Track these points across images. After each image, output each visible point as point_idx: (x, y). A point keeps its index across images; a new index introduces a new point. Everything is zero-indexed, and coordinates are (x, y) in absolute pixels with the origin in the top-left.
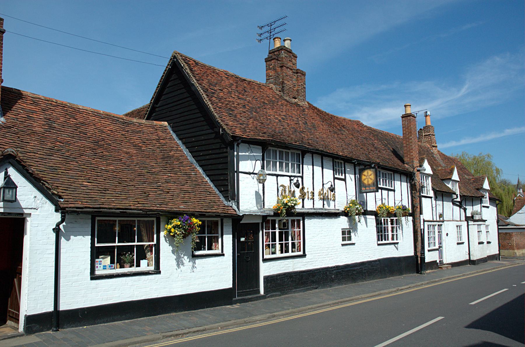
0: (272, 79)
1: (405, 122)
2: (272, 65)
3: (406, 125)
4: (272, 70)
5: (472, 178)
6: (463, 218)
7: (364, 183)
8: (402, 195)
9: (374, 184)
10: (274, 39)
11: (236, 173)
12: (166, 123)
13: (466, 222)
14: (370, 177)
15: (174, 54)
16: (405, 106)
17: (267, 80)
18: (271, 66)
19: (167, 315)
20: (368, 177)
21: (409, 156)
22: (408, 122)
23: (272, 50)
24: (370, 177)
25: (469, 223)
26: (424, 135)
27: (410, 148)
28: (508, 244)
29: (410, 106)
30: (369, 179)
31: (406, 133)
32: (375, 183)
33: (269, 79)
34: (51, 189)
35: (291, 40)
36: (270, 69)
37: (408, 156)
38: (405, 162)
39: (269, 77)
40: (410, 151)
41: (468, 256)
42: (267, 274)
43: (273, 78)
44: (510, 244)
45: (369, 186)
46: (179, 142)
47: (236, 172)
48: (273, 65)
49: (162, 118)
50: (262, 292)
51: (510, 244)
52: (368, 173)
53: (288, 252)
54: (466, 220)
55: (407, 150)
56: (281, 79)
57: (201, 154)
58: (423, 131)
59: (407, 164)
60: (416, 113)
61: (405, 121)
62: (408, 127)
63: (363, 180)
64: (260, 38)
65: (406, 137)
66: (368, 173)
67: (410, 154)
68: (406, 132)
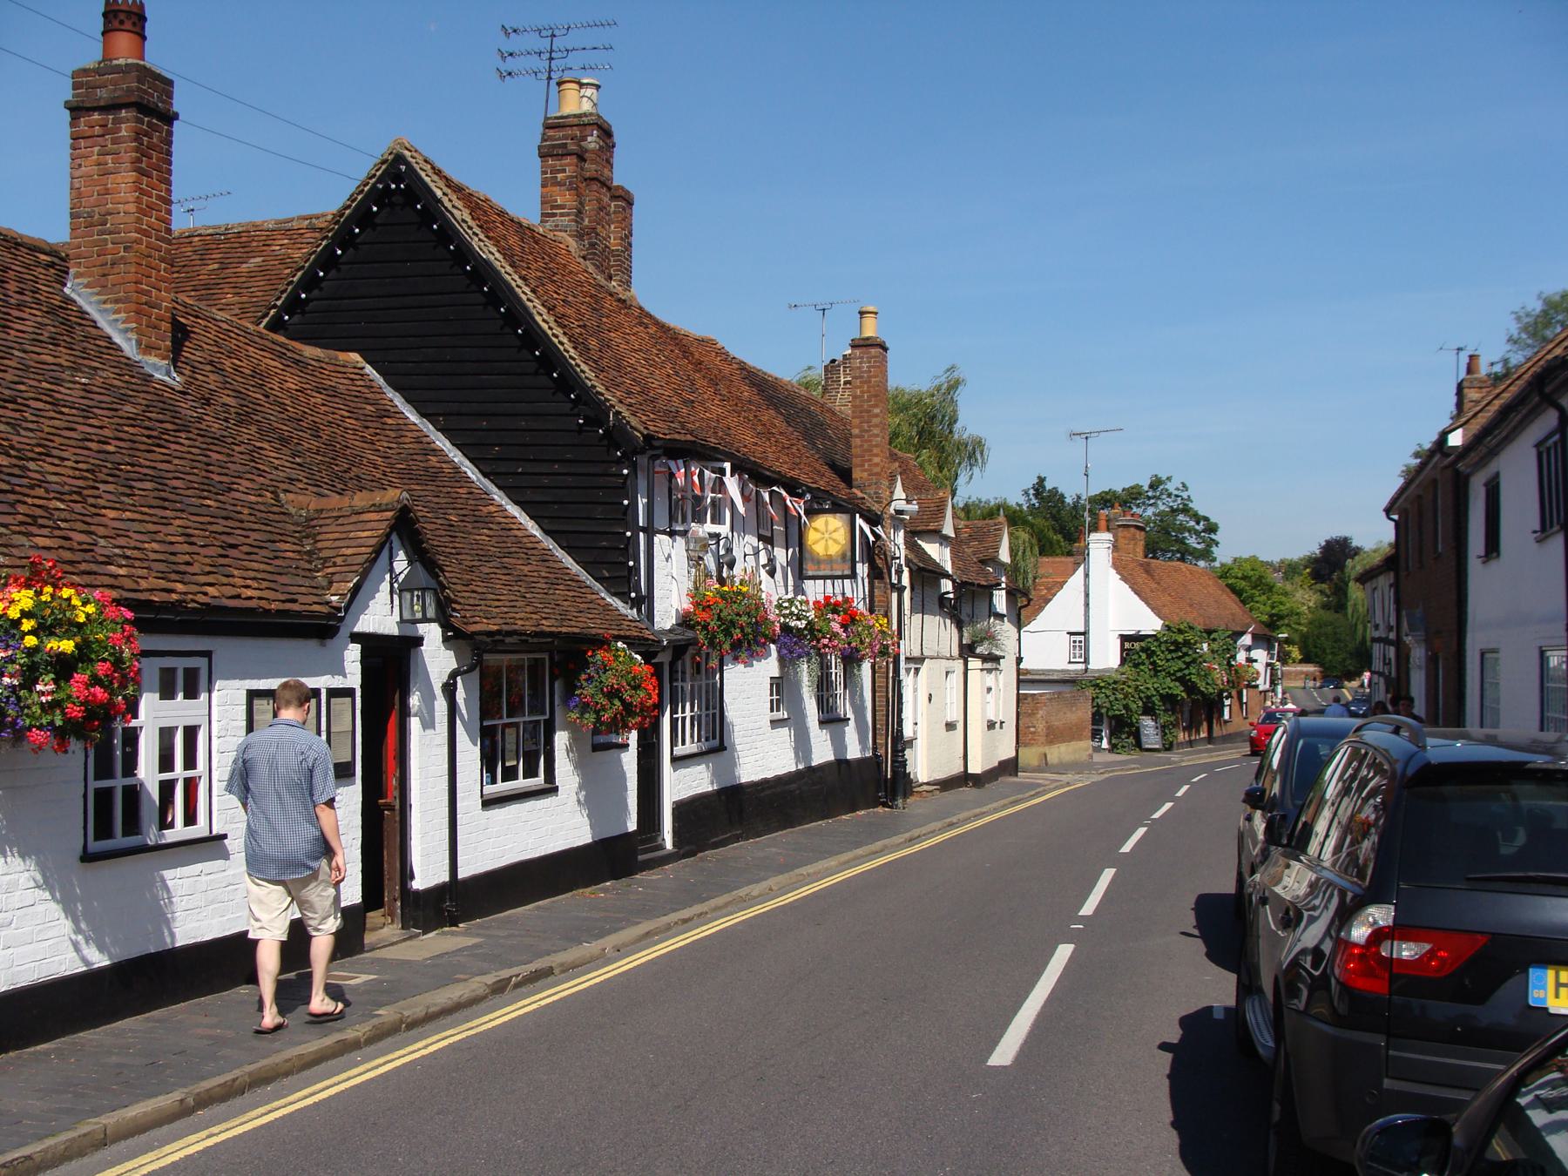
0: (562, 215)
1: (861, 363)
2: (564, 171)
3: (863, 372)
4: (562, 188)
5: (967, 527)
6: (956, 652)
7: (811, 552)
8: (1087, 605)
9: (844, 556)
10: (559, 84)
11: (641, 534)
12: (355, 357)
13: (962, 661)
14: (835, 535)
15: (398, 147)
16: (862, 313)
17: (543, 215)
18: (560, 176)
19: (564, 896)
20: (827, 536)
21: (866, 466)
22: (870, 362)
23: (556, 118)
24: (835, 535)
25: (970, 665)
26: (842, 380)
27: (870, 441)
28: (1029, 727)
29: (876, 313)
30: (830, 542)
31: (863, 396)
32: (849, 554)
33: (554, 215)
34: (446, 588)
35: (598, 87)
36: (560, 184)
37: (863, 465)
38: (854, 483)
39: (553, 207)
40: (871, 451)
41: (961, 762)
42: (677, 798)
43: (568, 214)
44: (1032, 729)
45: (830, 560)
46: (427, 427)
47: (644, 529)
48: (568, 174)
49: (311, 338)
50: (669, 845)
51: (1032, 729)
52: (827, 523)
53: (95, 789)
54: (961, 655)
55: (862, 446)
56: (587, 220)
57: (520, 470)
58: (842, 369)
59: (858, 487)
60: (822, 307)
61: (862, 358)
62: (869, 377)
63: (809, 543)
64: (504, 67)
65: (862, 406)
66: (827, 523)
67: (870, 460)
68: (862, 392)
